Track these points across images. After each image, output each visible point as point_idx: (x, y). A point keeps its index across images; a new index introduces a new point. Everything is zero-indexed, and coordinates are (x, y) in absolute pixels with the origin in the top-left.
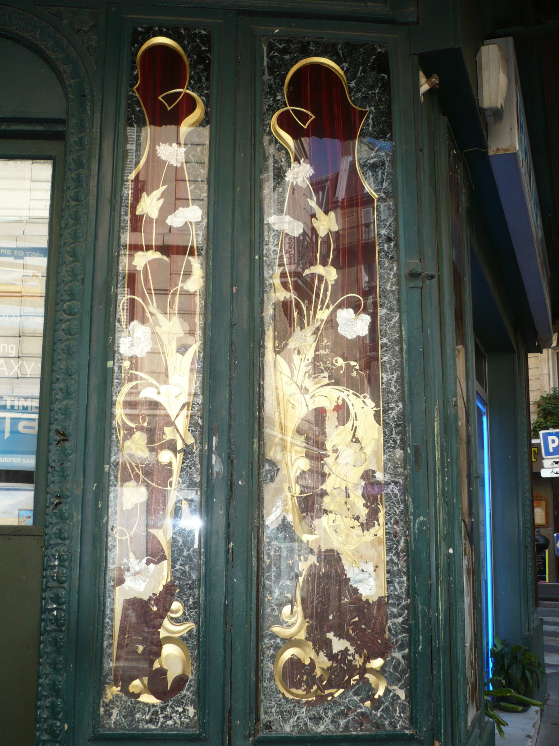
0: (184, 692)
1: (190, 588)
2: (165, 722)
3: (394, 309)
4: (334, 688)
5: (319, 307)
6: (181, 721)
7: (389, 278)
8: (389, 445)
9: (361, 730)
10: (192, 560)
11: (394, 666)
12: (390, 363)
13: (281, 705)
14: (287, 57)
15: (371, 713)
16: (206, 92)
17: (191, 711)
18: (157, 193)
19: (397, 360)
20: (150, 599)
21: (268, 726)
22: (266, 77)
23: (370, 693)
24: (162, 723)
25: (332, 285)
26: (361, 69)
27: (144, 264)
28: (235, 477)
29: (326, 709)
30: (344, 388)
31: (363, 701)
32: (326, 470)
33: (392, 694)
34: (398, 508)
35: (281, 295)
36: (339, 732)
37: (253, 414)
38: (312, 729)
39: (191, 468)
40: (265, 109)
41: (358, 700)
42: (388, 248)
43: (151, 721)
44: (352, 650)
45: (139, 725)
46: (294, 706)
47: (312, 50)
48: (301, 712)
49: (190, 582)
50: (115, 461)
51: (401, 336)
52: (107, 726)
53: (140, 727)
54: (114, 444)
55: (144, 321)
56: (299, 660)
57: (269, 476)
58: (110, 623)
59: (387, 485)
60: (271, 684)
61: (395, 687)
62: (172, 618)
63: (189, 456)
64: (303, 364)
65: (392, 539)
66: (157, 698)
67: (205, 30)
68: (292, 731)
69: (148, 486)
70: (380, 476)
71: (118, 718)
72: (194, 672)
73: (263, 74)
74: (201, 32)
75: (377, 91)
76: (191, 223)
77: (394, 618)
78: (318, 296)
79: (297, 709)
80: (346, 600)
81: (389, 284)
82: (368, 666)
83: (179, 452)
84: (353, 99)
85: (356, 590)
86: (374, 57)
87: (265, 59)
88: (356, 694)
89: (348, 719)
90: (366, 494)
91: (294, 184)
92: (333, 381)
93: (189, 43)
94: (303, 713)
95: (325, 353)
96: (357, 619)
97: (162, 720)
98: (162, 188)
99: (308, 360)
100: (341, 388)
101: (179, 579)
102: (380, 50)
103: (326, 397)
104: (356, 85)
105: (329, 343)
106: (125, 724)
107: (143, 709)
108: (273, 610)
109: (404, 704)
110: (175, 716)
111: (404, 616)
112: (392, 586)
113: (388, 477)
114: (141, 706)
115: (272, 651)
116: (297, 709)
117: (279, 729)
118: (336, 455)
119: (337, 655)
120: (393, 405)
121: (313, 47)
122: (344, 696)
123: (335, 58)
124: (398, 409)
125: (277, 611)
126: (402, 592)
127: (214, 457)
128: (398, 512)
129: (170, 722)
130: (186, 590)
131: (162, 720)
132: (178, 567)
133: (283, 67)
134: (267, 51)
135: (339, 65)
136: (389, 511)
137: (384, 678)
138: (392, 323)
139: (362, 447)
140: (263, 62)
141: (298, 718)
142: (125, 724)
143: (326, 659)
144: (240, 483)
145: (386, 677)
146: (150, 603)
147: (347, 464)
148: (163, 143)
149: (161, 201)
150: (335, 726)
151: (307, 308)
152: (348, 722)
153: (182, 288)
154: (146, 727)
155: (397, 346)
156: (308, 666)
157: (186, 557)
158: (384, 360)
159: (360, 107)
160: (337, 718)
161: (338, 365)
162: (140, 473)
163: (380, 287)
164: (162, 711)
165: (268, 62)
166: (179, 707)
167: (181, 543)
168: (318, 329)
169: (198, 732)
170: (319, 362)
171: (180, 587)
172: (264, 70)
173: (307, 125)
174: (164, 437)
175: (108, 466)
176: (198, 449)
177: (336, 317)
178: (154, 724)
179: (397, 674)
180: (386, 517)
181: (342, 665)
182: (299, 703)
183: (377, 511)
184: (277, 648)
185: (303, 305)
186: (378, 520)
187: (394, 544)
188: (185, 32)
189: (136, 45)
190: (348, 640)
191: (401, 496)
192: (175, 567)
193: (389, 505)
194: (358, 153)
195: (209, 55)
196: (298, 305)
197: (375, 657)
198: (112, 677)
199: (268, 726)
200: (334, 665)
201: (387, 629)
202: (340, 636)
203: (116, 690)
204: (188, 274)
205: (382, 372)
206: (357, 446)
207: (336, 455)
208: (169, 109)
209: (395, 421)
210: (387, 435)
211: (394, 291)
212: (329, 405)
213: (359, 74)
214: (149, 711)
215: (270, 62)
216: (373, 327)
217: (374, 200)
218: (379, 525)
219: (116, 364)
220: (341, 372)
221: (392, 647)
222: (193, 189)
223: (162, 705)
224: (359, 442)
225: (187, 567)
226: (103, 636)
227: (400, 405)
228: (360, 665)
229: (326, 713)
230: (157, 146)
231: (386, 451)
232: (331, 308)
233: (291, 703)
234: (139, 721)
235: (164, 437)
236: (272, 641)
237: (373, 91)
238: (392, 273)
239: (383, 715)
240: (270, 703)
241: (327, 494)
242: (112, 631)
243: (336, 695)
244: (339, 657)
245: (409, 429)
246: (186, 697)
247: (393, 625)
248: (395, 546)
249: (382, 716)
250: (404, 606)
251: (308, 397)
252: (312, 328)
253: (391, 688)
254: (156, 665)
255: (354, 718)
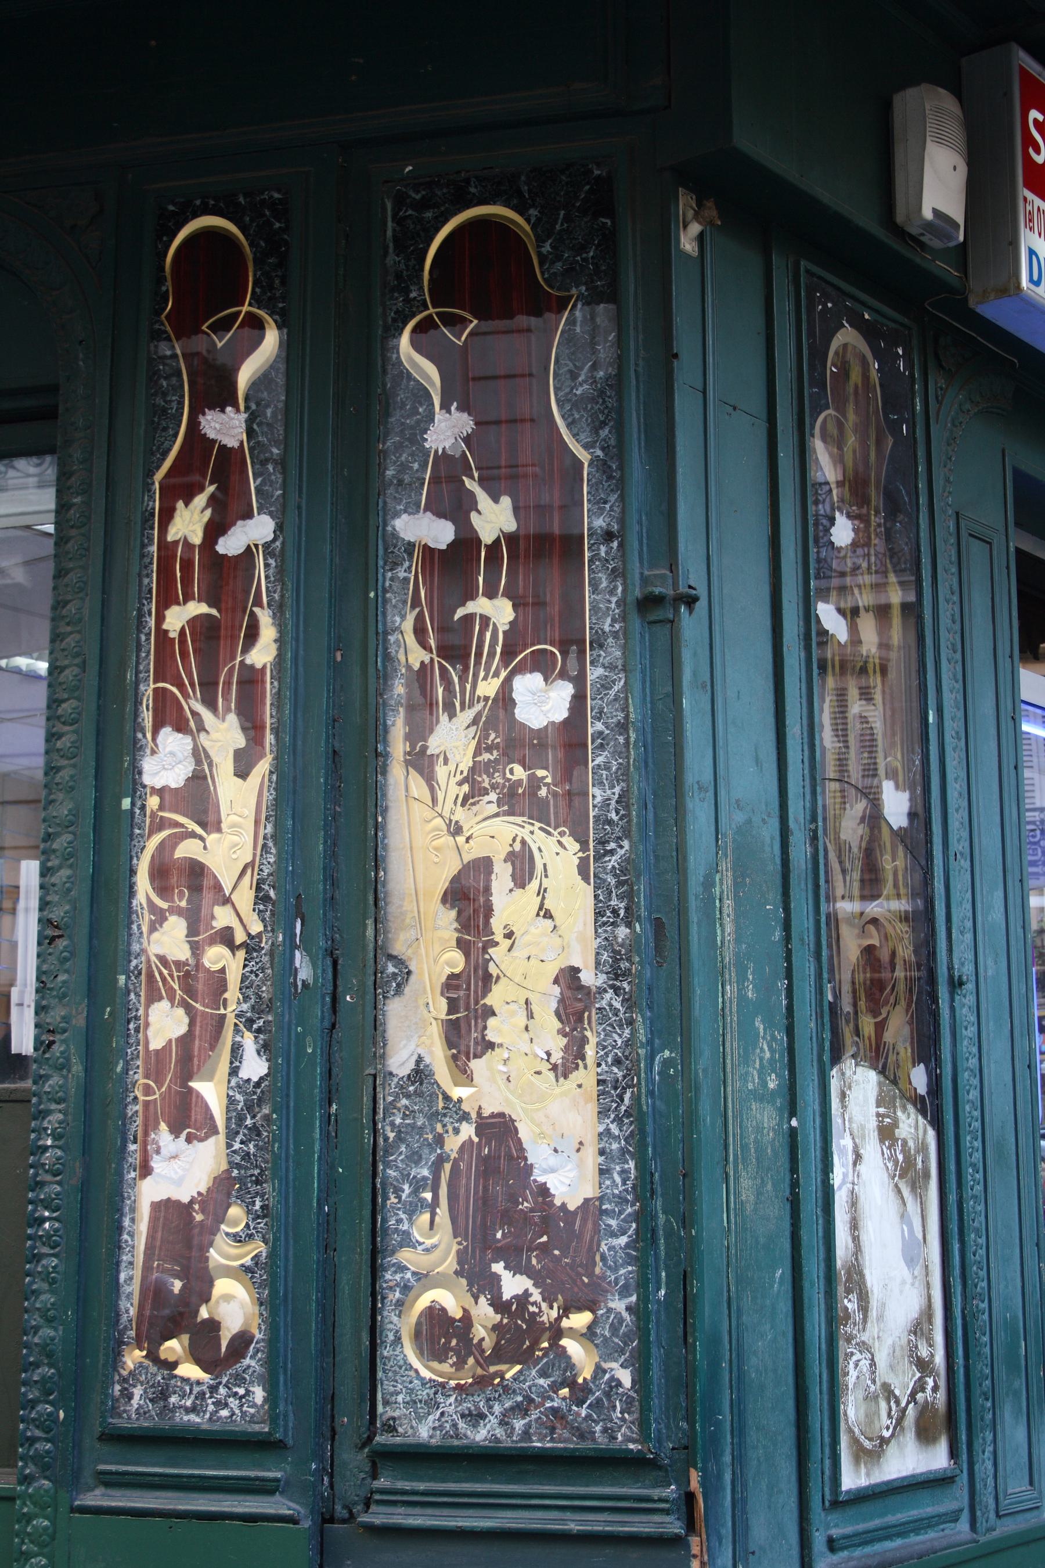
0: (247, 1361)
1: (257, 1182)
2: (217, 1412)
3: (617, 667)
4: (505, 1363)
5: (482, 674)
6: (241, 1412)
7: (608, 608)
8: (605, 919)
9: (552, 1440)
10: (259, 1134)
11: (612, 1324)
12: (608, 768)
13: (412, 1390)
14: (429, 215)
15: (570, 1410)
16: (281, 305)
17: (259, 1394)
18: (200, 500)
19: (621, 761)
20: (192, 1201)
21: (390, 1426)
22: (391, 259)
23: (568, 1373)
24: (211, 1414)
25: (504, 632)
26: (561, 216)
27: (181, 625)
28: (340, 989)
29: (490, 1399)
30: (525, 819)
31: (555, 1387)
32: (492, 969)
33: (607, 1376)
34: (620, 1036)
35: (417, 656)
36: (513, 1441)
37: (366, 874)
38: (465, 1435)
39: (257, 976)
40: (390, 320)
41: (546, 1386)
42: (607, 553)
43: (193, 1409)
44: (536, 1296)
45: (174, 1416)
46: (436, 1393)
47: (474, 194)
48: (448, 1403)
49: (257, 1172)
50: (137, 966)
51: (627, 717)
52: (125, 1415)
53: (178, 1419)
54: (135, 938)
55: (181, 727)
56: (443, 1310)
57: (394, 985)
58: (130, 1243)
59: (600, 993)
60: (397, 1353)
61: (614, 1365)
62: (227, 1234)
63: (255, 954)
64: (453, 781)
65: (609, 1093)
66: (205, 1371)
67: (279, 191)
68: (431, 1437)
69: (189, 1010)
70: (589, 978)
71: (142, 1402)
72: (263, 1328)
73: (386, 254)
74: (272, 197)
75: (591, 254)
76: (256, 546)
77: (611, 1237)
78: (479, 655)
79: (440, 1398)
80: (526, 1204)
81: (609, 620)
82: (565, 1323)
83: (239, 947)
84: (546, 276)
85: (544, 1190)
86: (587, 187)
87: (390, 224)
88: (543, 1374)
89: (528, 1419)
90: (562, 1012)
91: (440, 452)
92: (506, 808)
93: (252, 220)
94: (450, 1405)
95: (492, 758)
96: (545, 1238)
97: (211, 1408)
98: (211, 489)
99: (462, 772)
100: (519, 820)
101: (238, 1166)
102: (599, 172)
103: (493, 837)
104: (552, 247)
105: (498, 740)
106: (154, 1413)
107: (182, 1388)
108: (399, 1221)
109: (629, 1396)
110: (233, 1403)
111: (630, 1233)
112: (608, 1179)
113: (602, 977)
114: (179, 1384)
115: (397, 1295)
116: (440, 1398)
117: (410, 1432)
118: (510, 942)
119: (509, 1303)
120: (612, 845)
121: (476, 187)
122: (522, 1378)
123: (515, 201)
124: (622, 852)
125: (406, 1222)
126: (626, 1190)
127: (297, 954)
128: (619, 1042)
129: (224, 1413)
130: (249, 1185)
131: (211, 1408)
132: (237, 1146)
133: (422, 234)
134: (393, 209)
135: (521, 214)
136: (604, 1040)
137: (593, 1347)
138: (612, 692)
139: (555, 927)
140: (385, 231)
141: (442, 1414)
142: (154, 1413)
143: (491, 1310)
144: (348, 998)
145: (596, 1346)
146: (193, 1209)
147: (529, 958)
148: (210, 409)
149: (208, 513)
150: (506, 1431)
151: (460, 678)
152: (528, 1426)
153: (242, 662)
154: (186, 1418)
155: (621, 734)
156: (460, 1320)
157: (250, 1129)
158: (596, 762)
159: (559, 289)
160: (509, 1417)
161: (514, 778)
162: (176, 987)
163: (591, 628)
164: (211, 1393)
165: (394, 230)
166: (239, 1386)
167: (242, 1104)
168: (479, 715)
169: (267, 1430)
170: (480, 776)
171: (240, 1180)
172: (388, 247)
173: (463, 339)
174: (214, 924)
175: (124, 977)
176: (270, 943)
177: (511, 690)
178: (198, 1415)
179: (616, 1340)
180: (597, 1052)
181: (519, 1322)
182: (444, 1387)
183: (584, 1041)
184: (406, 1288)
185: (453, 674)
186: (583, 1058)
187: (612, 1101)
188: (245, 199)
189: (165, 239)
190: (529, 1277)
191: (625, 1013)
192: (232, 1146)
193: (604, 1030)
194: (554, 379)
195: (286, 237)
196: (444, 672)
197: (580, 1309)
198: (132, 1333)
199: (390, 1428)
200: (505, 1321)
201: (598, 1258)
202: (515, 1268)
203: (138, 1354)
204: (253, 634)
205: (593, 785)
206: (548, 923)
207: (510, 942)
208: (220, 345)
209: (615, 875)
210: (601, 901)
211: (617, 632)
212: (499, 853)
213: (558, 227)
214: (191, 1393)
215: (398, 229)
216: (578, 700)
217: (582, 464)
218: (586, 1067)
219: (139, 803)
220: (520, 791)
221: (607, 1291)
222: (260, 484)
223: (211, 1382)
224: (551, 917)
225: (251, 1146)
226: (118, 1264)
227: (626, 844)
228: (550, 1323)
229: (491, 1407)
230: (201, 416)
231: (600, 931)
232: (503, 674)
233: (431, 1387)
234: (173, 1410)
235: (214, 924)
236: (398, 1277)
237: (584, 255)
238: (614, 599)
239: (591, 1415)
240: (394, 1386)
241: (494, 1014)
242: (133, 1256)
243: (508, 1376)
244: (514, 1307)
245: (639, 889)
246: (251, 1371)
247: (609, 1249)
248: (614, 1105)
249: (588, 1417)
250: (629, 1215)
251: (461, 839)
252: (469, 715)
253: (606, 1366)
254: (204, 1313)
255: (540, 1418)
